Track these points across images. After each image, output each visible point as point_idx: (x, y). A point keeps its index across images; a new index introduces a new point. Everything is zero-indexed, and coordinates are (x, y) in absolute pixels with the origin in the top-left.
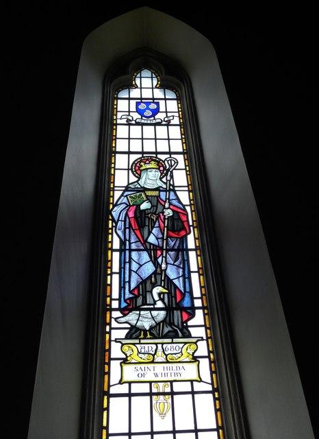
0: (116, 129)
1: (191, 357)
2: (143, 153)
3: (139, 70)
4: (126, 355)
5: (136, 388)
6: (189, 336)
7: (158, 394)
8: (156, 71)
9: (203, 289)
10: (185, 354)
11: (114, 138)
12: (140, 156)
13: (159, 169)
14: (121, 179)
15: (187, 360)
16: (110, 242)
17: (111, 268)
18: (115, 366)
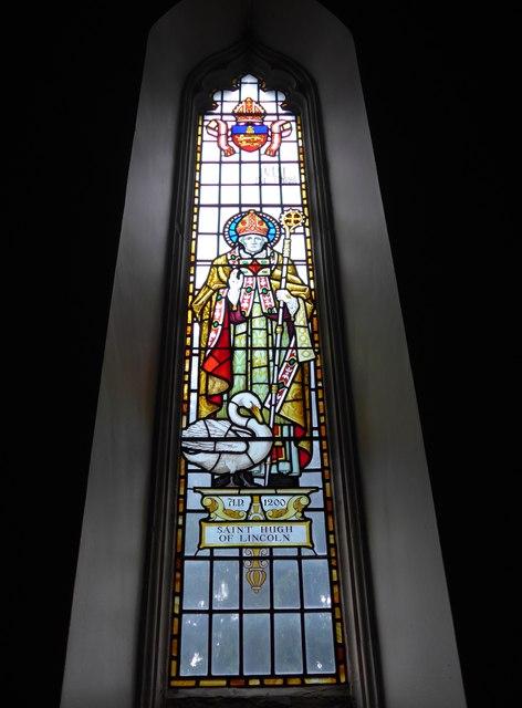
0: (198, 214)
1: (300, 515)
2: (240, 206)
9: (325, 454)
12: (236, 210)
14: (207, 247)
15: (294, 518)
17: (189, 382)
18: (192, 521)
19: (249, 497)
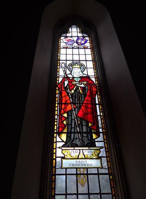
3: (70, 26)
4: (64, 155)
5: (69, 171)
6: (95, 146)
7: (81, 174)
8: (78, 26)
10: (94, 155)
11: (58, 76)
12: (72, 62)
13: (80, 68)
14: (61, 73)
15: (95, 157)
16: (54, 153)
19: (78, 151)
